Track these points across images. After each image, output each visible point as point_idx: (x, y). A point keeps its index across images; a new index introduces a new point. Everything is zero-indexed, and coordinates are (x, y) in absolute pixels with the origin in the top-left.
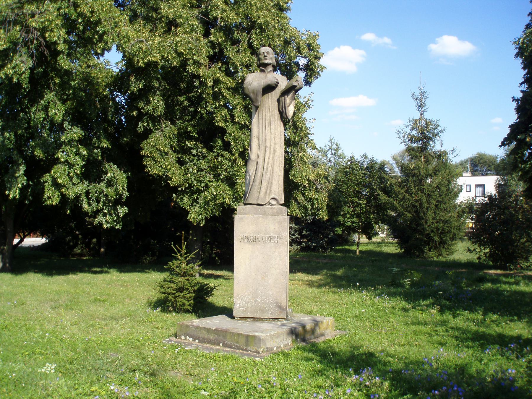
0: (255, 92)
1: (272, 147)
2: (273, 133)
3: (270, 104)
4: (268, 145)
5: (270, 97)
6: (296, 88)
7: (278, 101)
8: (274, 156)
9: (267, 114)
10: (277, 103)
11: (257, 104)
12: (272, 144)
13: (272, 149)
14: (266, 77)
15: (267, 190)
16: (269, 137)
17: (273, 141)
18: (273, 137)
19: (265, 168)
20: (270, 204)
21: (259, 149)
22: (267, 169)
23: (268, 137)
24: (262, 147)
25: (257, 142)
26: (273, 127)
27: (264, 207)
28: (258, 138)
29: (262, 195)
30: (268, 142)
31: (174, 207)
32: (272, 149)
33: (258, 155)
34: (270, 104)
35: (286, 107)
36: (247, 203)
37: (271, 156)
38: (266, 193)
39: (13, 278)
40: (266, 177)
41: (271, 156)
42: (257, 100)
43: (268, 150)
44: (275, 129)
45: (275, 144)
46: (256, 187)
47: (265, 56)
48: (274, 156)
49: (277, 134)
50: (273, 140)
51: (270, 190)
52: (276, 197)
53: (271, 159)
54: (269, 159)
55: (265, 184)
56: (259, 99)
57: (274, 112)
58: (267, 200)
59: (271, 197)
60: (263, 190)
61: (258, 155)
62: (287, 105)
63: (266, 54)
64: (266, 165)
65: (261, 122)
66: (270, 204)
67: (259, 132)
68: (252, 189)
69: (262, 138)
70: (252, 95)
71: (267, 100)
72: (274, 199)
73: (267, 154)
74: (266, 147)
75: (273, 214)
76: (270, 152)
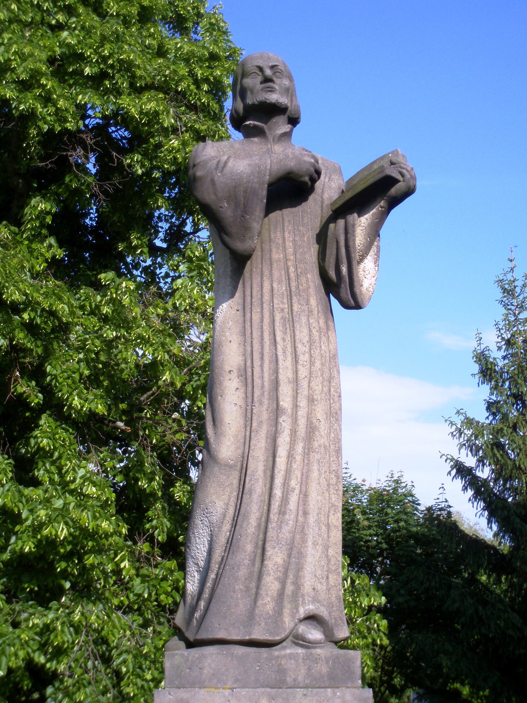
0: (239, 195)
1: (302, 413)
2: (304, 358)
3: (290, 250)
4: (286, 403)
5: (288, 227)
6: (394, 191)
7: (322, 238)
8: (308, 451)
9: (281, 288)
10: (314, 248)
11: (240, 246)
12: (303, 403)
13: (302, 422)
14: (269, 152)
15: (283, 584)
16: (290, 375)
17: (304, 391)
18: (303, 372)
19: (278, 492)
20: (299, 640)
21: (248, 417)
22: (285, 500)
23: (286, 373)
24: (262, 413)
25: (241, 394)
26: (302, 334)
27: (276, 652)
28: (246, 376)
29: (267, 603)
30: (286, 392)
31: (504, 527)
32: (302, 422)
33: (247, 442)
34: (290, 250)
35: (354, 263)
36: (203, 635)
37: (299, 447)
38: (281, 593)
39: (321, 221)
40: (281, 533)
41: (299, 447)
42: (246, 228)
43: (285, 423)
44: (311, 342)
45: (311, 400)
46: (243, 572)
47: (267, 80)
48: (308, 451)
49: (318, 364)
50: (304, 384)
51: (298, 586)
52: (323, 612)
53: (299, 458)
54: (290, 456)
55: (276, 557)
56: (256, 226)
57: (303, 280)
58: (288, 622)
59: (302, 612)
60: (271, 584)
61: (247, 442)
62: (356, 256)
63: (268, 72)
64: (278, 481)
65: (256, 317)
66: (299, 640)
67: (248, 355)
68: (225, 580)
69: (263, 377)
70: (227, 211)
71: (277, 236)
72: (312, 618)
73: (284, 440)
74: (277, 411)
75: (315, 683)
76: (294, 432)
